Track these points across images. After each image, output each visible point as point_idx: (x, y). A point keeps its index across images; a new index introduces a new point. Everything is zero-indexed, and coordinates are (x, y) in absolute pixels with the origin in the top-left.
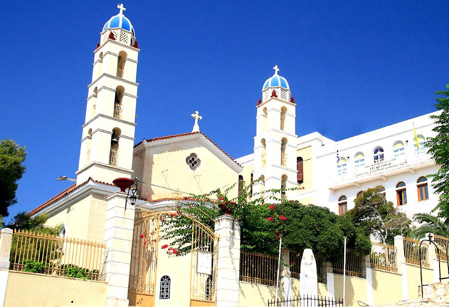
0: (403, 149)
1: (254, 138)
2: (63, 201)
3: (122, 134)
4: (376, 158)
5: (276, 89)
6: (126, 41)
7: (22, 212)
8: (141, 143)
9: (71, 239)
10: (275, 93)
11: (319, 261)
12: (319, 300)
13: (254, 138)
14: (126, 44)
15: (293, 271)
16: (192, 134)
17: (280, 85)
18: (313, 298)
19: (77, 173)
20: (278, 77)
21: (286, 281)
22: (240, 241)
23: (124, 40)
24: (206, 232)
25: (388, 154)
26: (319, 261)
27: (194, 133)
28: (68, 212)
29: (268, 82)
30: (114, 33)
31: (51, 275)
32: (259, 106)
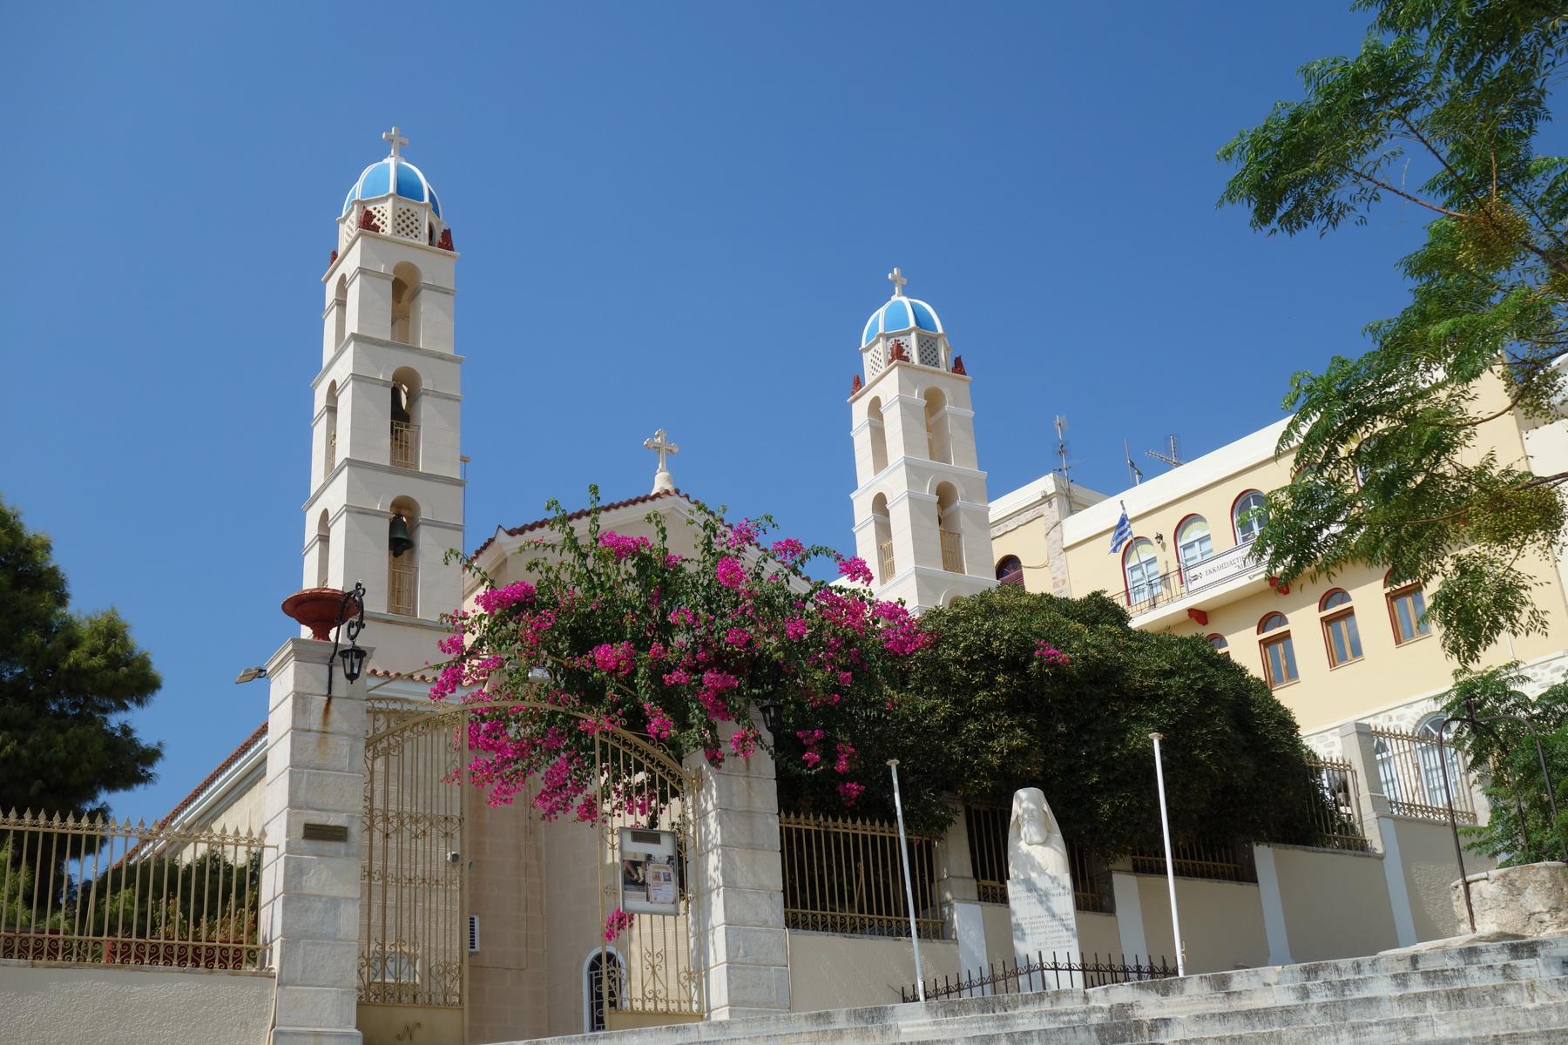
1: (852, 496)
5: (902, 339)
6: (416, 232)
8: (491, 541)
9: (128, 823)
10: (902, 350)
12: (1070, 969)
13: (852, 496)
14: (416, 241)
15: (984, 878)
17: (912, 324)
18: (1062, 961)
20: (905, 300)
21: (966, 918)
22: (774, 783)
23: (408, 230)
24: (610, 742)
27: (658, 495)
29: (877, 318)
30: (374, 213)
32: (857, 398)
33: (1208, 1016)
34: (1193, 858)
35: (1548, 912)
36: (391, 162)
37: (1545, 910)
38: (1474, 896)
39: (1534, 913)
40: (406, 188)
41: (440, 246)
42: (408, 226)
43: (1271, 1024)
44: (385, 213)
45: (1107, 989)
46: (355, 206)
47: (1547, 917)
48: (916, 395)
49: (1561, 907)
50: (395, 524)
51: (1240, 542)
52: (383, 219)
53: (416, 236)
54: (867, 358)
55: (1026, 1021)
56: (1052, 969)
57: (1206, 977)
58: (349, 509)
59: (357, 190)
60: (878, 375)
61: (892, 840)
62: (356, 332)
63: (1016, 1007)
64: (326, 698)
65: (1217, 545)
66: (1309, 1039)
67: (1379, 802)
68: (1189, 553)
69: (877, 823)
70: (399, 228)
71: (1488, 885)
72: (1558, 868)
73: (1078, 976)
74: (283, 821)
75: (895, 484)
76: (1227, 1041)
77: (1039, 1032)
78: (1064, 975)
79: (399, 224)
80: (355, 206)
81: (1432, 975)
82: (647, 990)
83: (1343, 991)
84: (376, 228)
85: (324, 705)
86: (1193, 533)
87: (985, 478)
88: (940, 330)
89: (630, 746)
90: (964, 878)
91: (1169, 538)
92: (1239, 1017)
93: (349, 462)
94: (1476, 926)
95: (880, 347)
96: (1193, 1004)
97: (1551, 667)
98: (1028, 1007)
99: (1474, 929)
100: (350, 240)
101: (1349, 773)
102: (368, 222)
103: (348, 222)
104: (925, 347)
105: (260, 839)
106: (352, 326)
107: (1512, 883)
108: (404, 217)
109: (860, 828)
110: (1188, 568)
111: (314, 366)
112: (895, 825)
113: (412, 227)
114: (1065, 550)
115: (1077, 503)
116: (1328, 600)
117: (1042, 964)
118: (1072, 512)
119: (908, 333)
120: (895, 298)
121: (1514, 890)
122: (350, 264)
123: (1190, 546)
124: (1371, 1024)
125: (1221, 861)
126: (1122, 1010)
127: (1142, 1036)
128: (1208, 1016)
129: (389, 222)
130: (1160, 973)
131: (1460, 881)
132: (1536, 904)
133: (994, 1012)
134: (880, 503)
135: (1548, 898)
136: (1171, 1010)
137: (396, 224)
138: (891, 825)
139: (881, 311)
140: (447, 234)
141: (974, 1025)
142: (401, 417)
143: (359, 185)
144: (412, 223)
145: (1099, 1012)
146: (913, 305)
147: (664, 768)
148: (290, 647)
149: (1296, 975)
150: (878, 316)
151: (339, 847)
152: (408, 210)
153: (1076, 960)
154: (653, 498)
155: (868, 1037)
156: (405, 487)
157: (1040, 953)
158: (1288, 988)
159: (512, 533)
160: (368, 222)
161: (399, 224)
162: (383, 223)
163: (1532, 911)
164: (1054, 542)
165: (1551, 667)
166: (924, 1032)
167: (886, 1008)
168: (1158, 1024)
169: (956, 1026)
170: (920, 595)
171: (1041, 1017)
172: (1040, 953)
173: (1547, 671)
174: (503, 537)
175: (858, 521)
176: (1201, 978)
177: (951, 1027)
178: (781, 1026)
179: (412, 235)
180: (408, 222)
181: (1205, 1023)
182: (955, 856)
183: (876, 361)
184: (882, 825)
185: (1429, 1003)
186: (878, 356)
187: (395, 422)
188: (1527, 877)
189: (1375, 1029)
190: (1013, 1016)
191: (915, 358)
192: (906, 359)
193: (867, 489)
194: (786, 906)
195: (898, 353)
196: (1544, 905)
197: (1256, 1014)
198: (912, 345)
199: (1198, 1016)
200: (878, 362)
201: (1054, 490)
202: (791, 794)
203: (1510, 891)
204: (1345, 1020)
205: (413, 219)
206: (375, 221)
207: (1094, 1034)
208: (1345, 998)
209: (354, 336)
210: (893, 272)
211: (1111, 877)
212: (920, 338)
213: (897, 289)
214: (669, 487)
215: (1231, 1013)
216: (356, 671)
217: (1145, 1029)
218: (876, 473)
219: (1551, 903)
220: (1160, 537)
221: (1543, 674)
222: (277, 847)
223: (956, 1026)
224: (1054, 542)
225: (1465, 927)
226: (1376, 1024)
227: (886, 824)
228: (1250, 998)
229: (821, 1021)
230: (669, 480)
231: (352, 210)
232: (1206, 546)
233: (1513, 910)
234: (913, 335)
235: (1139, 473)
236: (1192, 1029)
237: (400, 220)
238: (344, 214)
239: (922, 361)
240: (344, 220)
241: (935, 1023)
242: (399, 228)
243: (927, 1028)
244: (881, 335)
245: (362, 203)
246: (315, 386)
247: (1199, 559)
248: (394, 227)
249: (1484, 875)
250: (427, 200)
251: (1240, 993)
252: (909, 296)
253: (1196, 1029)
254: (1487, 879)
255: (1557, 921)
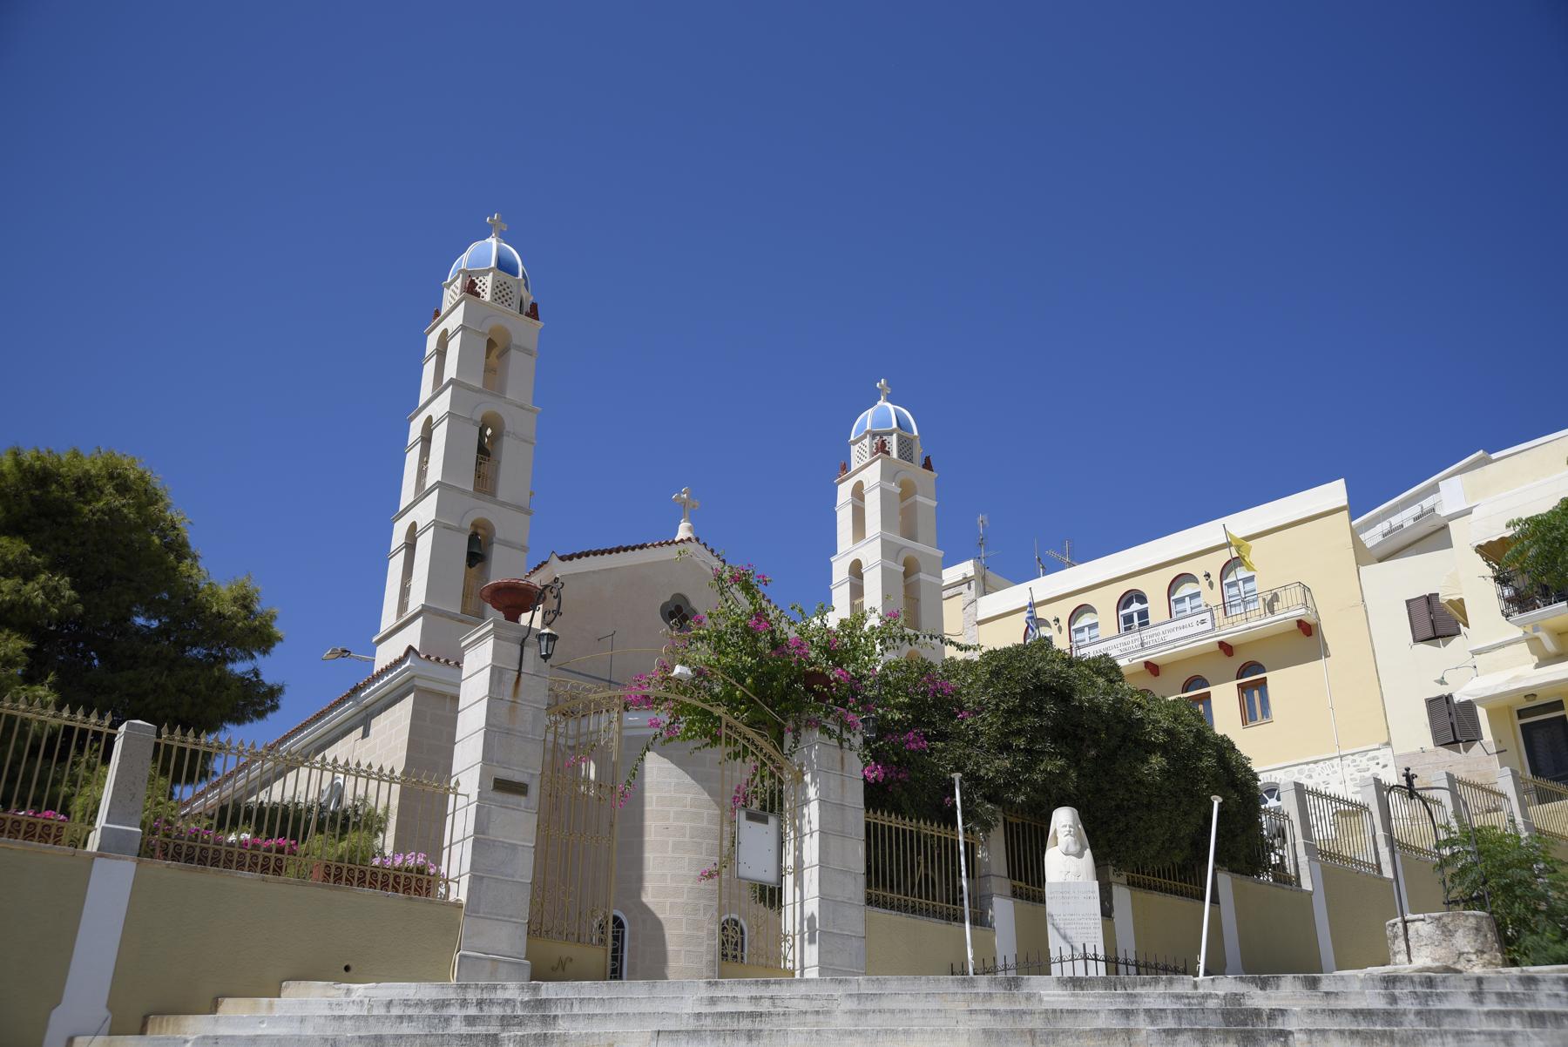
0: (1251, 579)
2: (349, 709)
3: (499, 534)
4: (1128, 619)
6: (510, 302)
7: (241, 727)
11: (954, 892)
16: (676, 543)
17: (895, 425)
18: (1090, 951)
19: (375, 639)
20: (889, 405)
21: (1003, 910)
23: (503, 299)
25: (1157, 606)
26: (954, 892)
27: (682, 541)
28: (365, 734)
30: (477, 281)
31: (1297, 618)
33: (1319, 1011)
34: (1170, 879)
35: (1475, 953)
36: (493, 242)
37: (1472, 951)
38: (1411, 932)
39: (1463, 953)
40: (505, 265)
41: (527, 315)
42: (503, 296)
43: (1375, 1024)
44: (486, 285)
45: (1213, 980)
46: (461, 275)
47: (1473, 957)
48: (894, 488)
49: (1485, 950)
50: (473, 539)
51: (1122, 631)
52: (483, 287)
53: (510, 305)
54: (854, 449)
55: (1151, 1000)
56: (1092, 959)
57: (1299, 978)
58: (435, 523)
59: (463, 261)
60: (863, 463)
61: (953, 841)
62: (455, 377)
63: (1134, 987)
64: (517, 673)
65: (1101, 632)
66: (1418, 1040)
67: (1311, 849)
68: (1079, 636)
69: (935, 824)
70: (496, 296)
71: (1422, 927)
72: (1482, 917)
73: (1102, 965)
74: (476, 773)
75: (871, 554)
76: (1347, 1034)
77: (1173, 1011)
78: (1091, 963)
79: (496, 293)
80: (461, 275)
81: (1505, 996)
82: (791, 942)
83: (1427, 1001)
84: (478, 295)
85: (515, 679)
86: (1085, 620)
87: (941, 556)
88: (916, 433)
89: (749, 740)
90: (1002, 877)
91: (1064, 623)
92: (1346, 1014)
93: (438, 485)
94: (1412, 958)
95: (867, 441)
96: (1296, 999)
97: (1368, 756)
98: (1145, 988)
99: (1410, 961)
100: (453, 302)
101: (1287, 822)
102: (471, 289)
103: (452, 287)
104: (903, 445)
105: (455, 788)
106: (451, 371)
107: (1445, 925)
108: (501, 288)
109: (926, 828)
110: (1079, 648)
111: (411, 405)
112: (956, 829)
113: (507, 297)
114: (980, 623)
115: (990, 586)
116: (1190, 684)
117: (1085, 954)
118: (985, 593)
119: (890, 434)
120: (879, 403)
121: (1447, 932)
122: (454, 321)
123: (1081, 630)
124: (1473, 1033)
125: (1196, 885)
126: (1236, 998)
127: (1262, 1022)
128: (1319, 1011)
129: (488, 290)
130: (1171, 971)
131: (1399, 919)
132: (1465, 945)
133: (1115, 990)
134: (856, 570)
135: (1475, 942)
136: (1276, 1002)
137: (494, 293)
138: (953, 829)
139: (870, 410)
140: (534, 306)
141: (1106, 1000)
142: (484, 451)
143: (465, 256)
144: (504, 290)
145: (1215, 998)
146: (896, 410)
147: (774, 761)
148: (491, 626)
149: (1376, 983)
150: (867, 415)
151: (522, 799)
152: (505, 283)
153: (1101, 953)
154: (676, 543)
155: (1015, 1002)
156: (484, 510)
157: (1084, 945)
158: (1379, 993)
159: (562, 559)
160: (471, 289)
161: (496, 293)
162: (483, 291)
163: (1462, 950)
164: (969, 615)
165: (1368, 756)
166: (1064, 1002)
167: (1022, 979)
168: (1276, 1013)
169: (1091, 999)
170: (493, 659)
171: (1165, 998)
172: (1084, 945)
173: (1364, 759)
174: (555, 559)
175: (835, 580)
176: (1294, 977)
177: (1087, 999)
178: (930, 985)
179: (506, 304)
180: (504, 293)
181: (1317, 1017)
182: (993, 853)
183: (862, 452)
184: (939, 826)
185: (1513, 1020)
186: (864, 448)
187: (480, 456)
188: (1457, 922)
189: (1476, 1037)
190: (1141, 995)
191: (895, 454)
192: (888, 453)
193: (844, 556)
194: (869, 885)
195: (882, 448)
196: (1471, 947)
197: (1361, 1013)
198: (893, 443)
199: (1311, 1010)
200: (864, 453)
201: (973, 574)
202: (875, 796)
203: (1443, 932)
204: (1439, 1026)
205: (508, 291)
206: (477, 288)
207: (1220, 1016)
208: (1428, 1008)
209: (451, 381)
210: (880, 382)
211: (1111, 888)
212: (900, 438)
213: (882, 397)
214: (690, 535)
215: (1339, 1010)
216: (549, 652)
217: (1265, 1018)
218: (853, 544)
219: (1478, 945)
220: (1057, 620)
221: (1361, 761)
222: (468, 796)
223: (1091, 999)
224: (969, 615)
225: (1402, 957)
226: (1479, 1033)
227: (949, 827)
228: (1346, 999)
229: (966, 984)
230: (690, 529)
231: (458, 277)
232: (1094, 632)
233: (1445, 948)
234: (895, 436)
235: (1043, 567)
236: (1305, 1020)
237: (497, 290)
238: (449, 280)
239: (900, 456)
240: (451, 284)
241: (1073, 995)
242: (496, 296)
243: (1066, 999)
244: (868, 432)
245: (468, 272)
246: (412, 419)
247: (1087, 641)
248: (492, 295)
249: (1421, 916)
250: (520, 276)
251: (1337, 994)
252: (892, 403)
253: (1308, 1021)
254: (1423, 920)
255: (1482, 961)
